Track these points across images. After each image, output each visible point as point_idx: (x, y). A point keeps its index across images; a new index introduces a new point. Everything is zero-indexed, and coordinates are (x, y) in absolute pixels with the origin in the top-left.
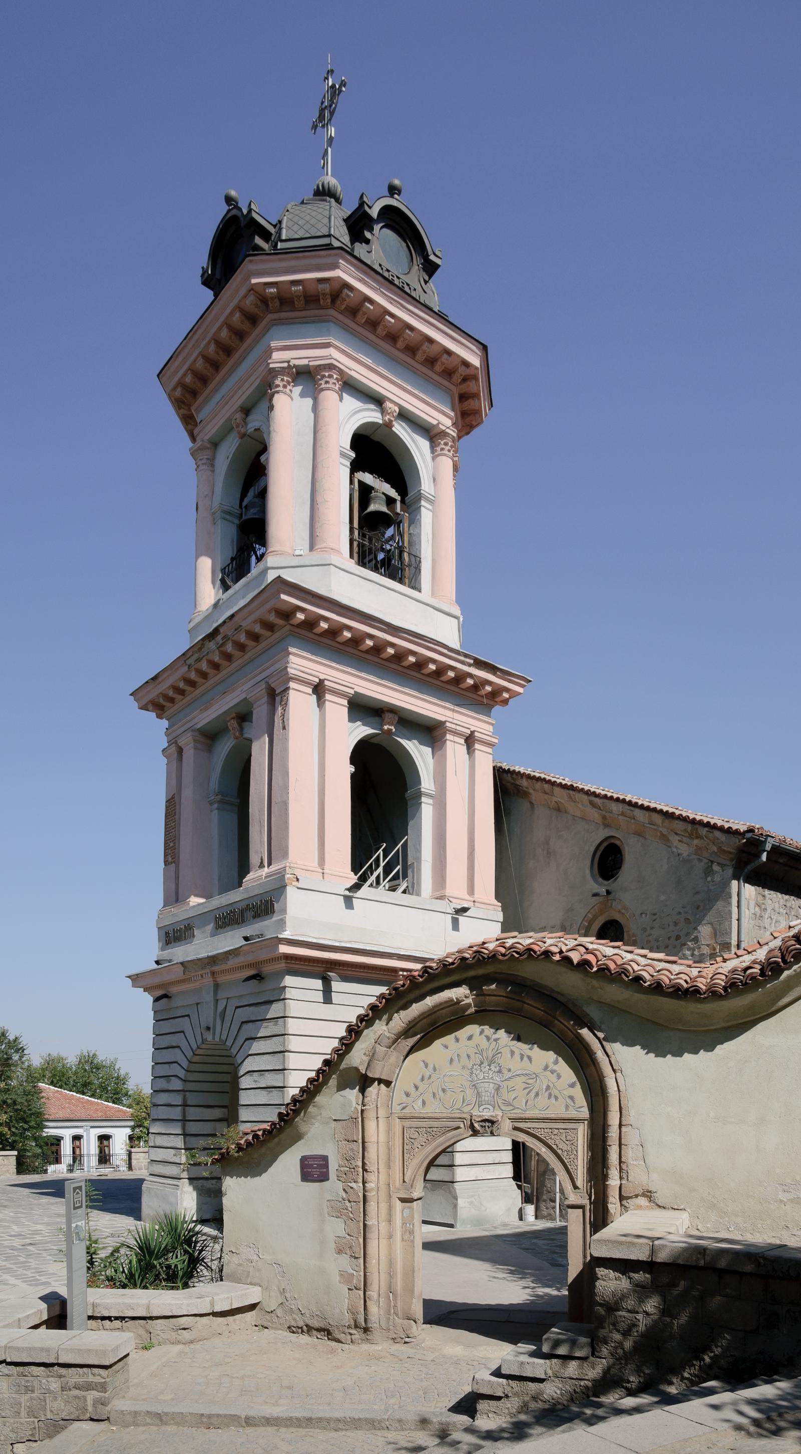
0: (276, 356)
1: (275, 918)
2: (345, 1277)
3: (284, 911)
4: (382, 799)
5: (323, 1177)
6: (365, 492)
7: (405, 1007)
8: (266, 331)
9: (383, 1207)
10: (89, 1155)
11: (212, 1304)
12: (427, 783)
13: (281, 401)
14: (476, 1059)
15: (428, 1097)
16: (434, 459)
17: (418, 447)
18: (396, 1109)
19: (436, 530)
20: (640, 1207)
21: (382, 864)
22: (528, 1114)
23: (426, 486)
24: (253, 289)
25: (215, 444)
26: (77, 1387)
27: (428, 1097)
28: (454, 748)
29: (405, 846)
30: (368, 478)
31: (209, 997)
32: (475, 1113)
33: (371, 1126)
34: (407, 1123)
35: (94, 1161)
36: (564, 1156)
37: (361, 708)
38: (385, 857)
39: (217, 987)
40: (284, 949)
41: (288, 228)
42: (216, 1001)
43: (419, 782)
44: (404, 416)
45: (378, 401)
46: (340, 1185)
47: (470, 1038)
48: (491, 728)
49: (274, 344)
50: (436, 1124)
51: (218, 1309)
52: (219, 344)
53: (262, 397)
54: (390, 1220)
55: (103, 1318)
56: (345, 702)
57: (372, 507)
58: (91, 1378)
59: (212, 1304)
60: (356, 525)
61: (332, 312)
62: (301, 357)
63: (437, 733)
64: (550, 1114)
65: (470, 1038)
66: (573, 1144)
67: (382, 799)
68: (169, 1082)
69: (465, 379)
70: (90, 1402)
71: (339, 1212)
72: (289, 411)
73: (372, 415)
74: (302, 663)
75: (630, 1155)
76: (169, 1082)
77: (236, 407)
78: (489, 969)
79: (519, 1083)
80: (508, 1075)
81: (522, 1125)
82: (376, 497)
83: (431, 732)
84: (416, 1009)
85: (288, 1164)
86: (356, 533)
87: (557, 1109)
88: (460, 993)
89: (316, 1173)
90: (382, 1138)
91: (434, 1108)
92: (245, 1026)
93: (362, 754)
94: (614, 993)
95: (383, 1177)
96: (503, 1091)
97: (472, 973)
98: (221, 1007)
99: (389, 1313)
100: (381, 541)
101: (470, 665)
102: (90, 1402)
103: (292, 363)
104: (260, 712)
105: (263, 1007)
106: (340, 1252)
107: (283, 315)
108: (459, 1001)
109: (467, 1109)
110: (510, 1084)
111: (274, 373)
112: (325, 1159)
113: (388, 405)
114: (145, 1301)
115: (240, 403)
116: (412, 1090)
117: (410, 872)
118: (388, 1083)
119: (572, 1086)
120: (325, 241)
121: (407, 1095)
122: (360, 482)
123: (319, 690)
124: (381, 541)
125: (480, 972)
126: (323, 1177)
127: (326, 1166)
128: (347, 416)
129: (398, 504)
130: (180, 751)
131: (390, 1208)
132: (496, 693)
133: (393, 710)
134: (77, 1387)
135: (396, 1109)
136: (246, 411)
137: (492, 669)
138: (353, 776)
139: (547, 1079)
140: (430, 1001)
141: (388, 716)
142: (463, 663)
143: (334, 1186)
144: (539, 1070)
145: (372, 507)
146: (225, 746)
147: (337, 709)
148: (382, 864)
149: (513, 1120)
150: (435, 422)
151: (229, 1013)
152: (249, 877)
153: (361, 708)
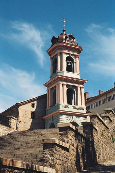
17: (73, 57)
28: (79, 89)
30: (68, 61)
44: (72, 55)
45: (69, 54)
83: (76, 87)
124: (70, 69)
128: (65, 56)
130: (49, 91)
138: (67, 93)
146: (53, 91)
147: (65, 86)
153: (67, 86)
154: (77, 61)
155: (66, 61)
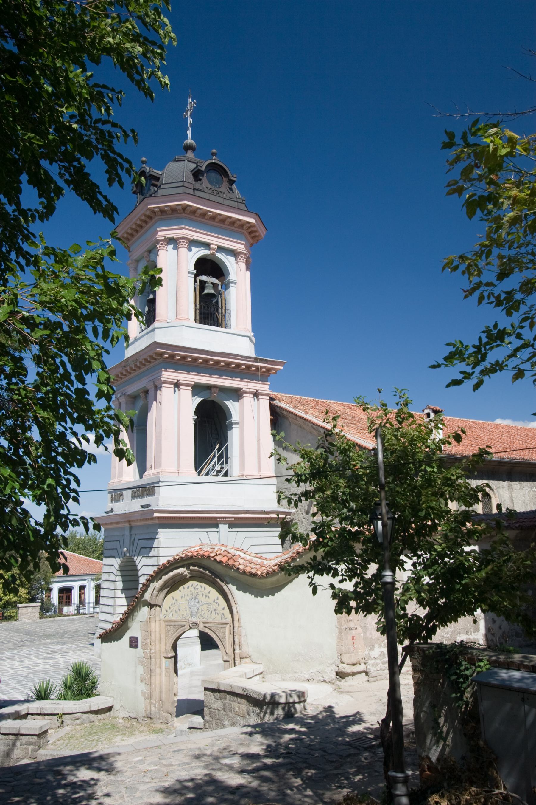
0: (160, 233)
1: (156, 496)
2: (143, 693)
3: (159, 494)
4: (212, 426)
5: (136, 647)
6: (203, 284)
7: (166, 574)
8: (156, 222)
9: (158, 661)
10: (89, 603)
11: (90, 707)
12: (235, 418)
13: (162, 253)
14: (190, 597)
15: (174, 612)
16: (237, 263)
17: (229, 261)
18: (163, 617)
19: (239, 295)
20: (246, 663)
21: (217, 456)
22: (209, 621)
23: (232, 277)
24: (149, 209)
25: (138, 261)
26: (26, 744)
27: (174, 612)
29: (226, 449)
30: (204, 278)
31: (127, 533)
32: (190, 620)
33: (153, 625)
34: (167, 623)
35: (92, 605)
36: (222, 639)
37: (197, 389)
38: (218, 452)
39: (131, 528)
40: (156, 515)
41: (166, 177)
42: (131, 535)
43: (231, 416)
44: (221, 249)
45: (207, 245)
46: (142, 651)
47: (188, 588)
48: (268, 386)
49: (158, 229)
50: (176, 624)
51: (92, 709)
52: (136, 224)
53: (153, 251)
54: (160, 667)
55: (45, 715)
56: (190, 388)
57: (206, 292)
58: (31, 740)
59: (90, 707)
60: (198, 302)
61: (184, 215)
62: (170, 234)
63: (240, 393)
64: (216, 621)
65: (188, 588)
66: (224, 633)
67: (212, 426)
68: (109, 576)
69: (249, 227)
70: (30, 750)
71: (142, 663)
72: (166, 258)
73: (203, 252)
74: (168, 375)
75: (242, 639)
76: (109, 576)
77: (145, 249)
78: (192, 561)
79: (205, 607)
80: (201, 604)
81: (207, 625)
82: (209, 286)
84: (165, 578)
85: (125, 640)
86: (198, 306)
87: (218, 619)
88: (181, 570)
89: (134, 644)
90: (158, 630)
91: (176, 617)
92: (142, 550)
93: (200, 410)
94: (232, 573)
95: (158, 647)
96: (200, 610)
97: (186, 562)
98: (133, 539)
99: (159, 710)
100: (210, 310)
101: (253, 362)
102: (30, 750)
103: (167, 236)
104: (151, 393)
105: (150, 541)
106: (142, 681)
107: (162, 217)
108: (182, 574)
109: (187, 618)
110: (202, 607)
111: (158, 242)
112: (137, 638)
113: (212, 246)
114: (62, 706)
115: (146, 248)
116: (168, 609)
117: (229, 460)
118: (160, 606)
119: (223, 609)
120: (181, 184)
121: (167, 611)
122: (200, 281)
123: (177, 385)
124: (210, 310)
125: (189, 562)
126: (136, 647)
127: (137, 642)
129: (220, 286)
131: (161, 661)
132: (269, 370)
133: (216, 387)
134: (26, 744)
135: (163, 617)
136: (150, 251)
137: (266, 361)
139: (215, 606)
140: (171, 574)
141: (213, 390)
142: (249, 361)
143: (140, 650)
144: (212, 602)
145: (206, 292)
147: (186, 393)
148: (217, 456)
149: (204, 623)
150: (235, 248)
151: (136, 541)
152: (146, 473)
154: (239, 273)
155: (196, 276)
